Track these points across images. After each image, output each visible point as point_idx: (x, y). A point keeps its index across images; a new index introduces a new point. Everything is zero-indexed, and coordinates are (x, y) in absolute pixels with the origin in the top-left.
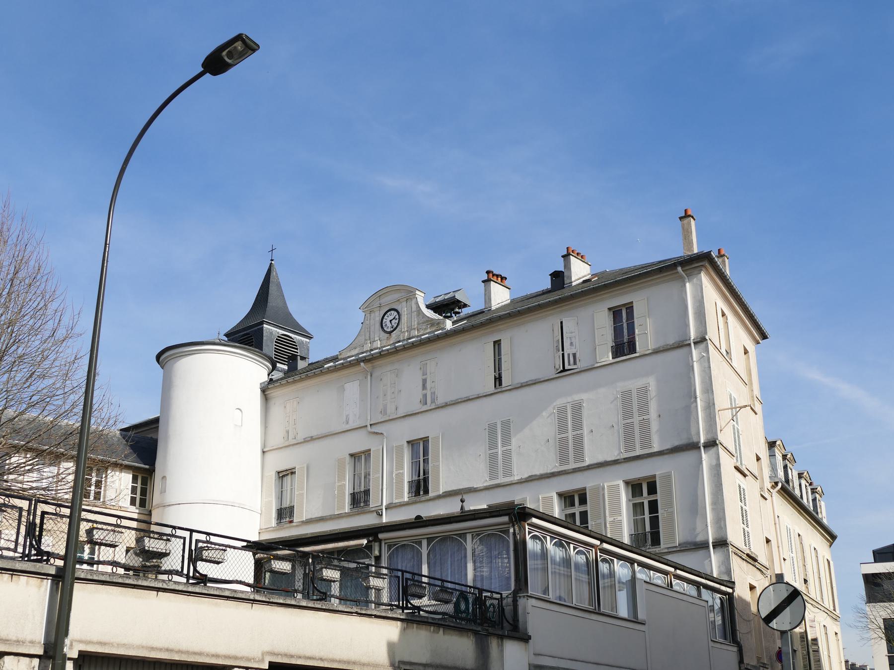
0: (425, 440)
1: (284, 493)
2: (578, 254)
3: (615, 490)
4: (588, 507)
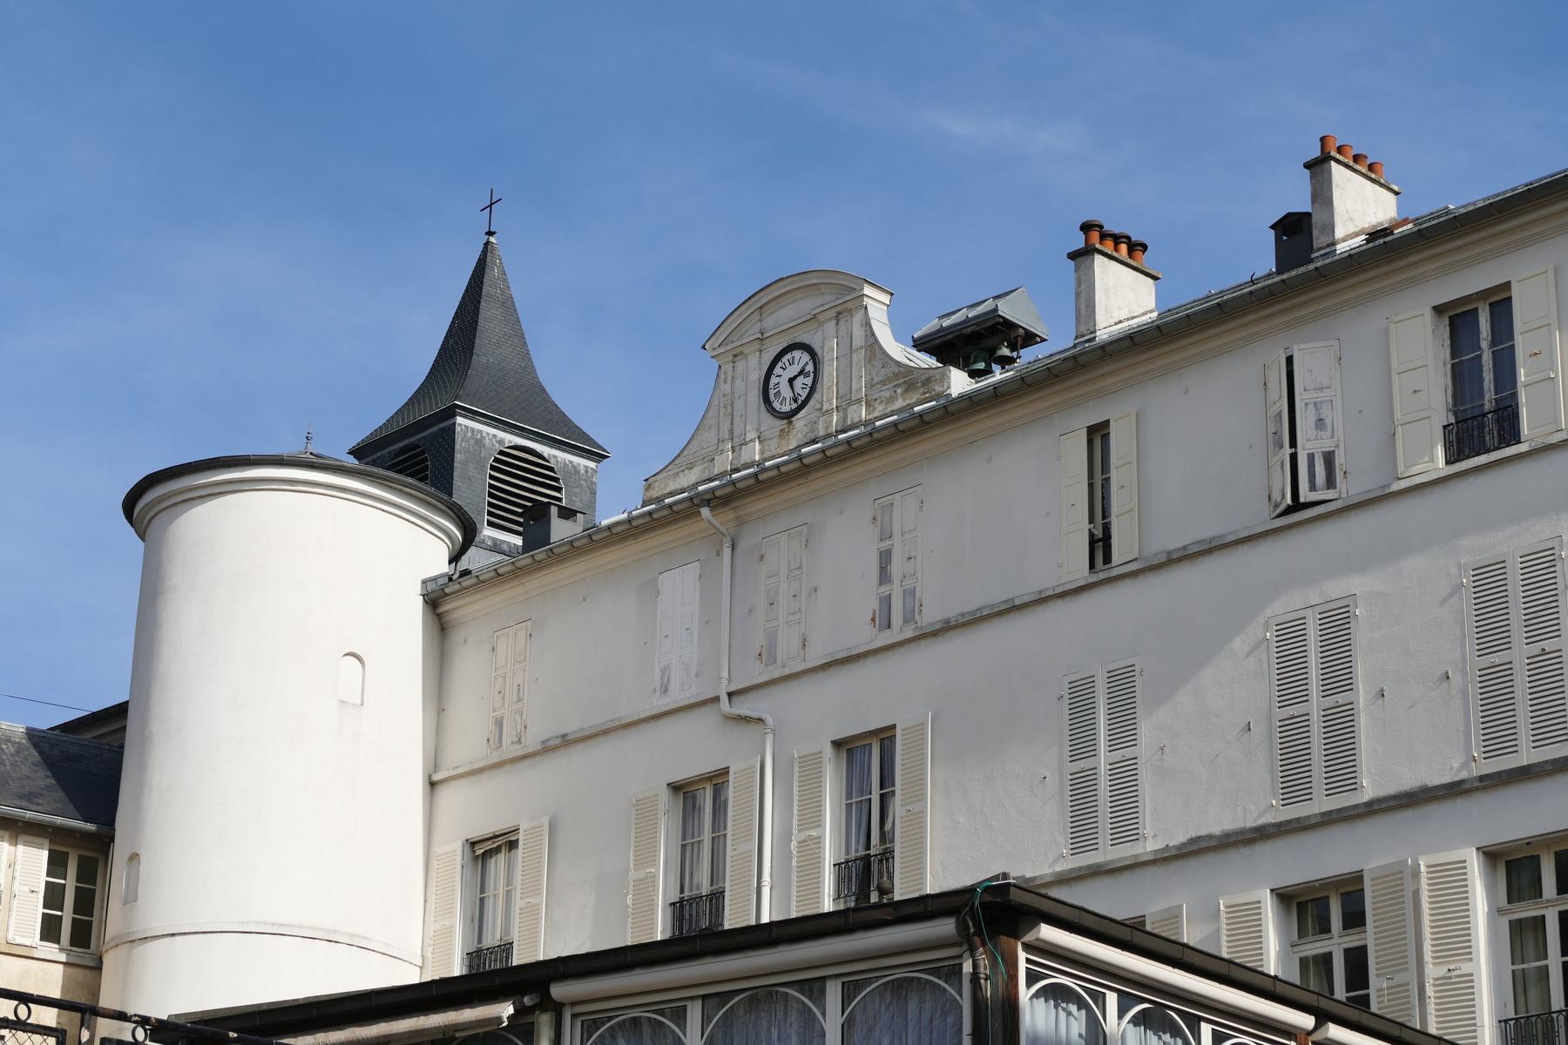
0: (885, 736)
1: (489, 904)
2: (1356, 158)
3: (1451, 878)
4: (1370, 937)
